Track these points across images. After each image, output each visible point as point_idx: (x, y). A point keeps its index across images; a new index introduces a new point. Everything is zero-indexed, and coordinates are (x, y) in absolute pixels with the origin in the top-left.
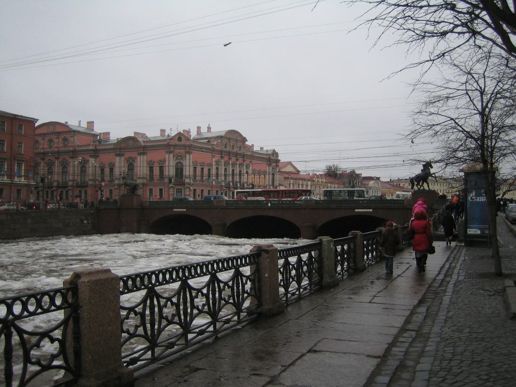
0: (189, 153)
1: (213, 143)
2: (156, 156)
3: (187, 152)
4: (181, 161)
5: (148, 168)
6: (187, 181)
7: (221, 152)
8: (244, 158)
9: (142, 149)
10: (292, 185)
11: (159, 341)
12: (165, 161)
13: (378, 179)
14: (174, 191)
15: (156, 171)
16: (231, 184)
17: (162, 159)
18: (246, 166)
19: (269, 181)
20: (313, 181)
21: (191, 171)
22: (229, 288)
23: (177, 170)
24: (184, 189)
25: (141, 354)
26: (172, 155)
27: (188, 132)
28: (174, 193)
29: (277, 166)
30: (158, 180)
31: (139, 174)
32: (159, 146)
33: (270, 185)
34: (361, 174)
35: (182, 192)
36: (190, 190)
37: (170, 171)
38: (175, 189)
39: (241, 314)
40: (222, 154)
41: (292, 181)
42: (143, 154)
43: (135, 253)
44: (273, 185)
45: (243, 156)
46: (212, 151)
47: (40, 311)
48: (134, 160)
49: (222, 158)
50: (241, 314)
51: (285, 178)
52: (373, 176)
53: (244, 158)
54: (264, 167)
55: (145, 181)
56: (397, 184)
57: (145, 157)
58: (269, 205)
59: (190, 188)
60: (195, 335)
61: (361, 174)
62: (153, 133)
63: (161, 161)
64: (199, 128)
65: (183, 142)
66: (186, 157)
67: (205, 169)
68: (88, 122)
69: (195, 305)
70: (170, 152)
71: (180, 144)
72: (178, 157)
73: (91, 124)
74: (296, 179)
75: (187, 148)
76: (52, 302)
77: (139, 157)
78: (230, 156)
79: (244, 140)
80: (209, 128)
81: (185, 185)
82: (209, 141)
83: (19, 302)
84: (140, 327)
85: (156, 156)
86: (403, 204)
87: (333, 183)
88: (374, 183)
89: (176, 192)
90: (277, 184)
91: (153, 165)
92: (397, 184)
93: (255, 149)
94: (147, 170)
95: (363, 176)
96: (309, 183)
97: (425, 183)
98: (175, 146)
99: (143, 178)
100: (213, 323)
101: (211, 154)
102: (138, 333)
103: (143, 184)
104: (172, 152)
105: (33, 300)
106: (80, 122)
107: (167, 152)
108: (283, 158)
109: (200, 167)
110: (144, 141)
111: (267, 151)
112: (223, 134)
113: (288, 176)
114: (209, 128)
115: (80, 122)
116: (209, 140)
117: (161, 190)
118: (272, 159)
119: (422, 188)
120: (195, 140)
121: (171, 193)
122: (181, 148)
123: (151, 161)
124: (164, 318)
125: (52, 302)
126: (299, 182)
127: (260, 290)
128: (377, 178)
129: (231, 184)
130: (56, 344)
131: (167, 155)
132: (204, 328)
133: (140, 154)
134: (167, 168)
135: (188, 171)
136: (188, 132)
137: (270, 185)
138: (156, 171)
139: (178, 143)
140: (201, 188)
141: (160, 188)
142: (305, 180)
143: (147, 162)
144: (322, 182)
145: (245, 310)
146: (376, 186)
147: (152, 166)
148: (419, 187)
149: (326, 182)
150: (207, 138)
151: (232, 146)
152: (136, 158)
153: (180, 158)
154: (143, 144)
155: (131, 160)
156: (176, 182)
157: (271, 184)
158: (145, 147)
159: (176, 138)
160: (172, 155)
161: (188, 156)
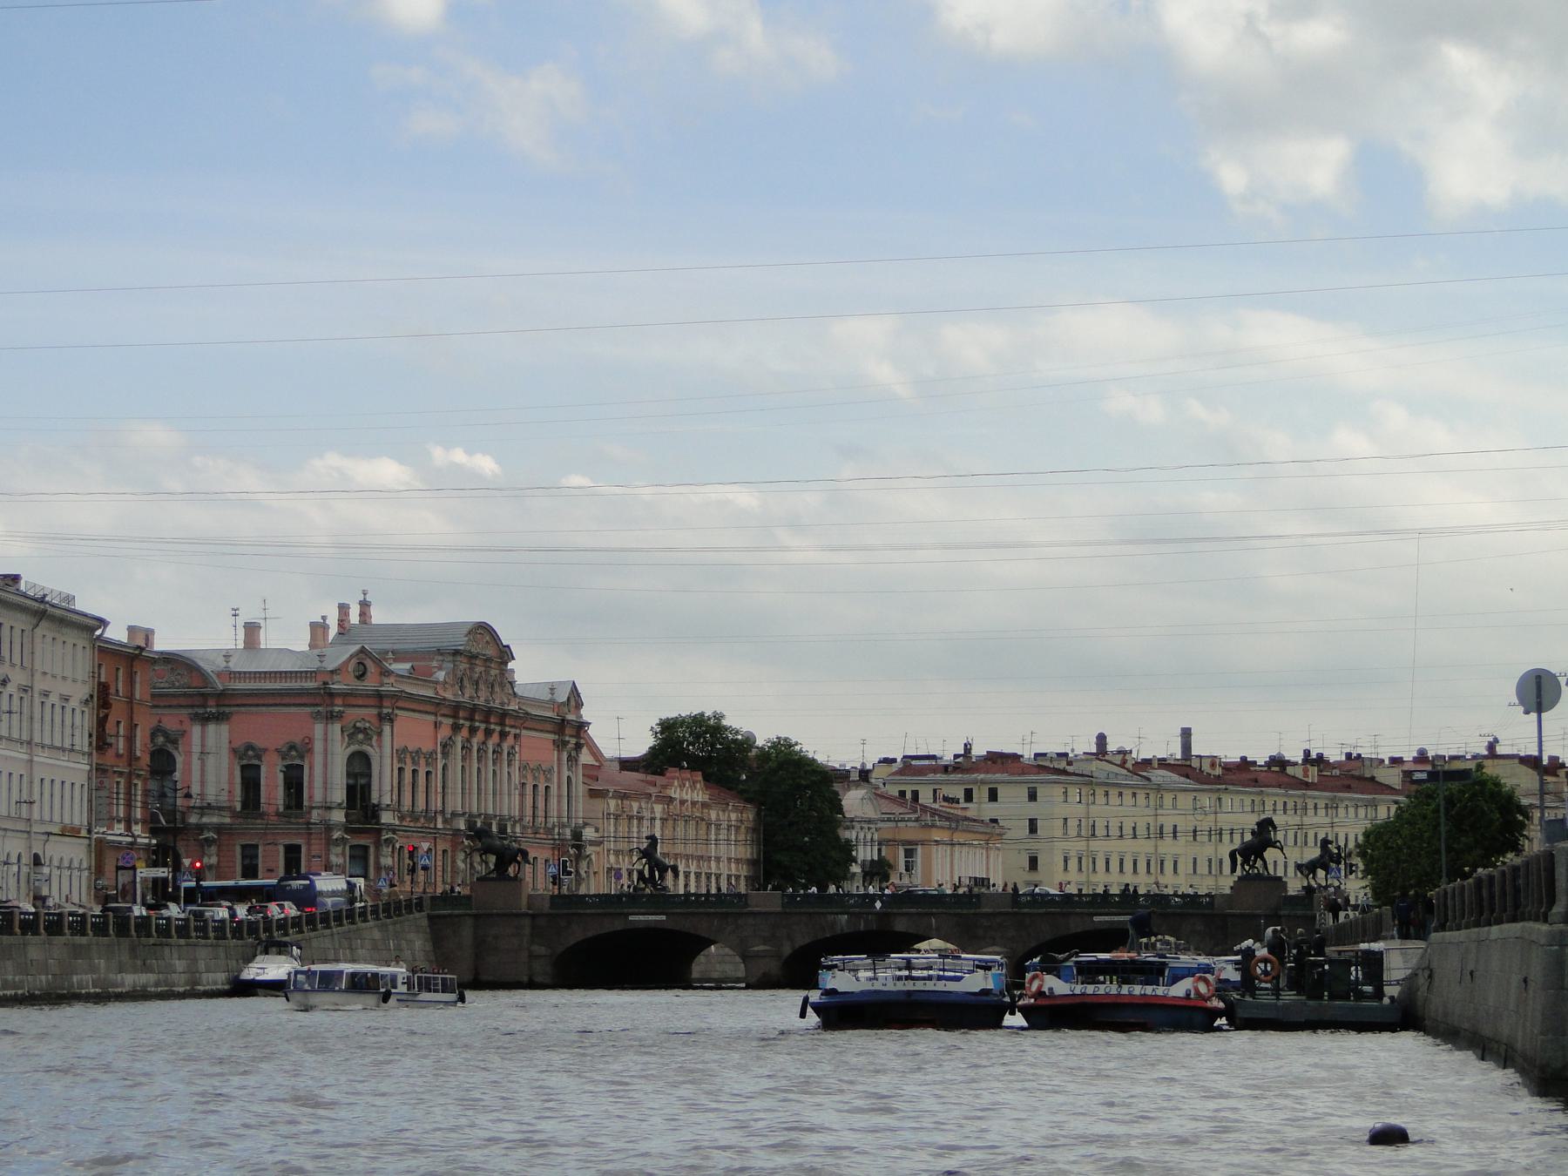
2: (271, 730)
3: (381, 718)
4: (366, 748)
8: (455, 716)
15: (273, 791)
17: (297, 740)
23: (351, 790)
24: (378, 844)
26: (337, 727)
30: (278, 814)
31: (195, 789)
37: (328, 782)
40: (381, 707)
42: (219, 718)
43: (104, 1077)
45: (504, 715)
49: (456, 728)
53: (455, 716)
56: (902, 793)
57: (224, 728)
58: (878, 905)
63: (292, 747)
66: (380, 734)
68: (152, 631)
70: (331, 717)
73: (968, 748)
75: (339, 701)
77: (196, 730)
86: (1211, 904)
91: (259, 757)
92: (902, 793)
101: (431, 718)
106: (1186, 734)
115: (1186, 734)
122: (304, 700)
123: (250, 747)
131: (319, 729)
133: (205, 720)
138: (273, 791)
141: (288, 842)
143: (234, 751)
147: (256, 762)
152: (184, 733)
153: (361, 736)
158: (222, 696)
160: (337, 727)
161: (387, 729)
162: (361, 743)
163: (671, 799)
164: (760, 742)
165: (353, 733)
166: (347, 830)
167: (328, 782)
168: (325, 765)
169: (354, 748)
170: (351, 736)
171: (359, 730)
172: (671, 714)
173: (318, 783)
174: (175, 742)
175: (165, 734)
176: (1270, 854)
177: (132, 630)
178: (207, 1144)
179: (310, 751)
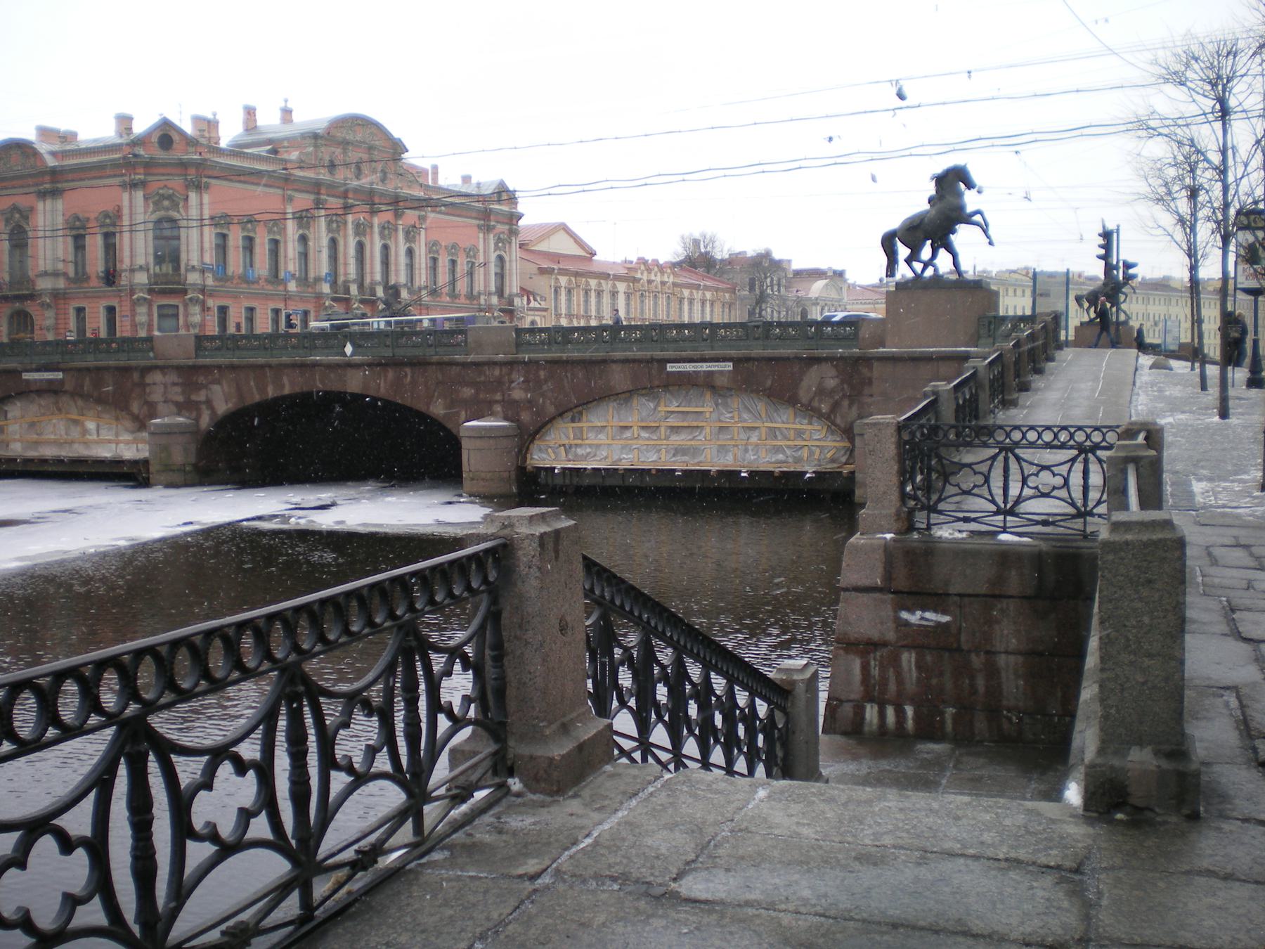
0: (199, 187)
1: (285, 156)
2: (91, 200)
4: (175, 215)
5: (70, 240)
6: (193, 278)
7: (316, 187)
9: (47, 178)
10: (593, 294)
11: (323, 851)
12: (118, 214)
13: (840, 275)
14: (150, 314)
16: (354, 289)
17: (109, 208)
18: (407, 233)
19: (579, 305)
20: (635, 280)
21: (206, 245)
22: (465, 669)
24: (186, 306)
25: (259, 911)
26: (139, 195)
27: (209, 122)
28: (151, 320)
29: (513, 232)
32: (100, 166)
33: (490, 294)
34: (789, 261)
35: (177, 316)
36: (205, 309)
38: (155, 309)
39: (427, 808)
41: (563, 281)
42: (55, 193)
44: (500, 292)
45: (397, 203)
46: (286, 181)
47: (51, 732)
48: (27, 214)
50: (427, 808)
51: (543, 271)
52: (823, 266)
54: (464, 232)
55: (61, 284)
57: (59, 204)
59: (203, 304)
60: (269, 921)
61: (789, 261)
62: (95, 129)
63: (107, 216)
64: (250, 112)
65: (178, 153)
67: (258, 241)
69: (443, 701)
70: (134, 185)
71: (165, 160)
72: (167, 201)
74: (577, 274)
76: (49, 714)
77: (40, 206)
78: (318, 193)
79: (397, 148)
80: (287, 113)
81: (185, 292)
82: (275, 151)
83: (27, 694)
84: (255, 814)
85: (91, 200)
87: (698, 287)
88: (827, 285)
89: (161, 316)
90: (515, 290)
93: (443, 181)
94: (65, 249)
95: (796, 266)
96: (621, 287)
97: (942, 252)
98: (150, 165)
99: (56, 274)
100: (300, 880)
101: (279, 192)
102: (251, 834)
103: (57, 295)
104: (143, 184)
105: (71, 687)
107: (123, 186)
108: (533, 213)
109: (241, 234)
110: (54, 154)
111: (479, 185)
112: (321, 127)
113: (552, 266)
114: (287, 113)
116: (275, 147)
117: (111, 310)
118: (493, 210)
119: (929, 272)
120: (237, 150)
121: (142, 318)
124: (338, 768)
125: (49, 714)
126: (588, 284)
127: (501, 693)
128: (835, 272)
129: (354, 289)
130: (81, 854)
131: (126, 196)
132: (372, 838)
133: (43, 195)
134: (126, 236)
135: (197, 246)
136: (210, 125)
137: (490, 294)
139: (160, 154)
140: (272, 305)
142: (606, 276)
144: (663, 283)
145: (442, 791)
146: (834, 295)
148: (918, 266)
149: (674, 284)
150: (269, 142)
151: (352, 168)
152: (32, 209)
153: (166, 203)
154: (51, 162)
155: (17, 216)
156: (156, 283)
157: (493, 289)
158: (54, 173)
159: (155, 139)
160: (139, 195)
161: (193, 196)
162: (167, 209)
163: (638, 280)
164: (81, 137)
165: (157, 200)
166: (150, 291)
167: (138, 249)
168: (202, 242)
169: (162, 213)
170: (156, 204)
171: (163, 197)
172: (220, 126)
173: (126, 253)
174: (26, 218)
175: (19, 211)
176: (963, 236)
177: (197, 120)
178: (744, 921)
179: (120, 217)
